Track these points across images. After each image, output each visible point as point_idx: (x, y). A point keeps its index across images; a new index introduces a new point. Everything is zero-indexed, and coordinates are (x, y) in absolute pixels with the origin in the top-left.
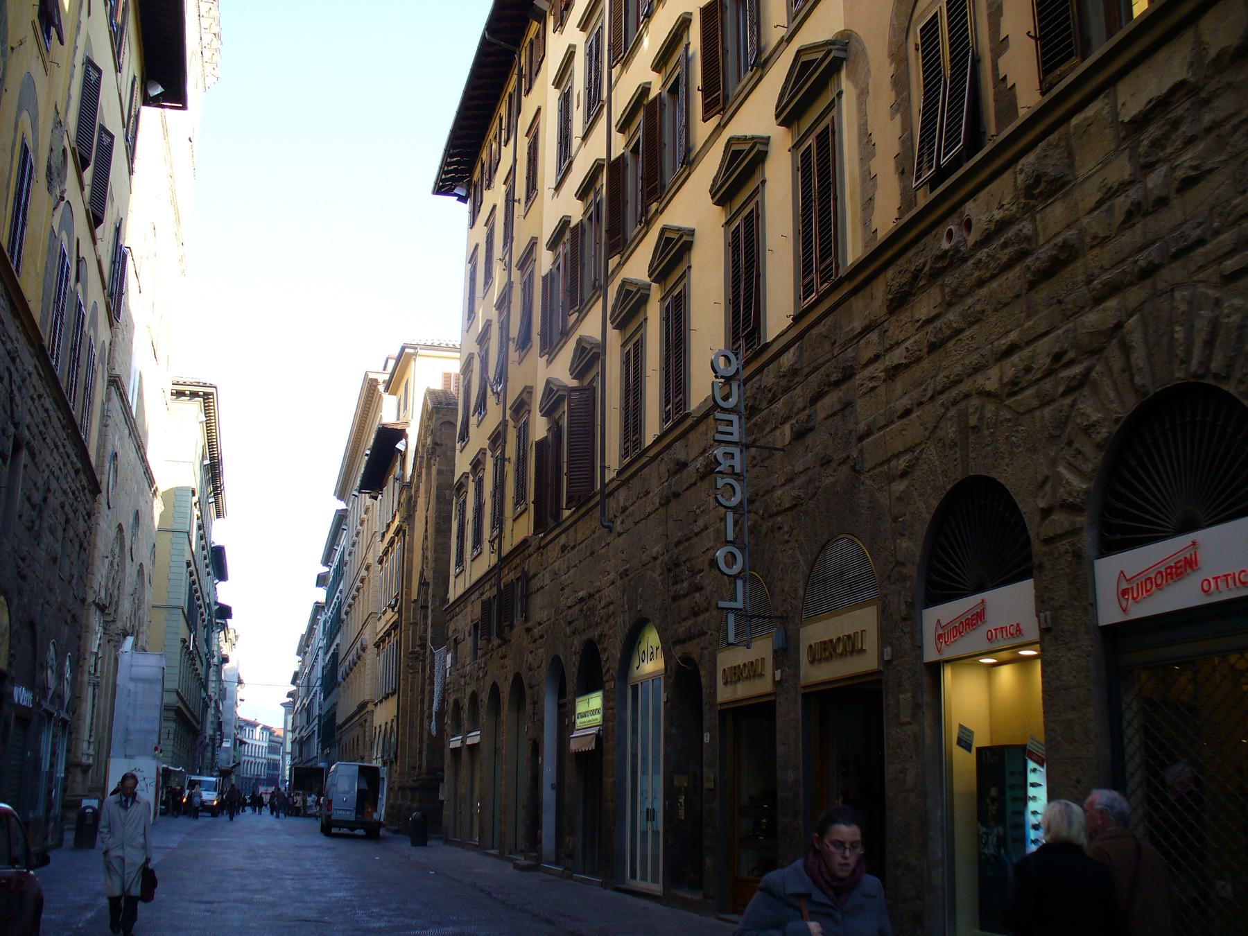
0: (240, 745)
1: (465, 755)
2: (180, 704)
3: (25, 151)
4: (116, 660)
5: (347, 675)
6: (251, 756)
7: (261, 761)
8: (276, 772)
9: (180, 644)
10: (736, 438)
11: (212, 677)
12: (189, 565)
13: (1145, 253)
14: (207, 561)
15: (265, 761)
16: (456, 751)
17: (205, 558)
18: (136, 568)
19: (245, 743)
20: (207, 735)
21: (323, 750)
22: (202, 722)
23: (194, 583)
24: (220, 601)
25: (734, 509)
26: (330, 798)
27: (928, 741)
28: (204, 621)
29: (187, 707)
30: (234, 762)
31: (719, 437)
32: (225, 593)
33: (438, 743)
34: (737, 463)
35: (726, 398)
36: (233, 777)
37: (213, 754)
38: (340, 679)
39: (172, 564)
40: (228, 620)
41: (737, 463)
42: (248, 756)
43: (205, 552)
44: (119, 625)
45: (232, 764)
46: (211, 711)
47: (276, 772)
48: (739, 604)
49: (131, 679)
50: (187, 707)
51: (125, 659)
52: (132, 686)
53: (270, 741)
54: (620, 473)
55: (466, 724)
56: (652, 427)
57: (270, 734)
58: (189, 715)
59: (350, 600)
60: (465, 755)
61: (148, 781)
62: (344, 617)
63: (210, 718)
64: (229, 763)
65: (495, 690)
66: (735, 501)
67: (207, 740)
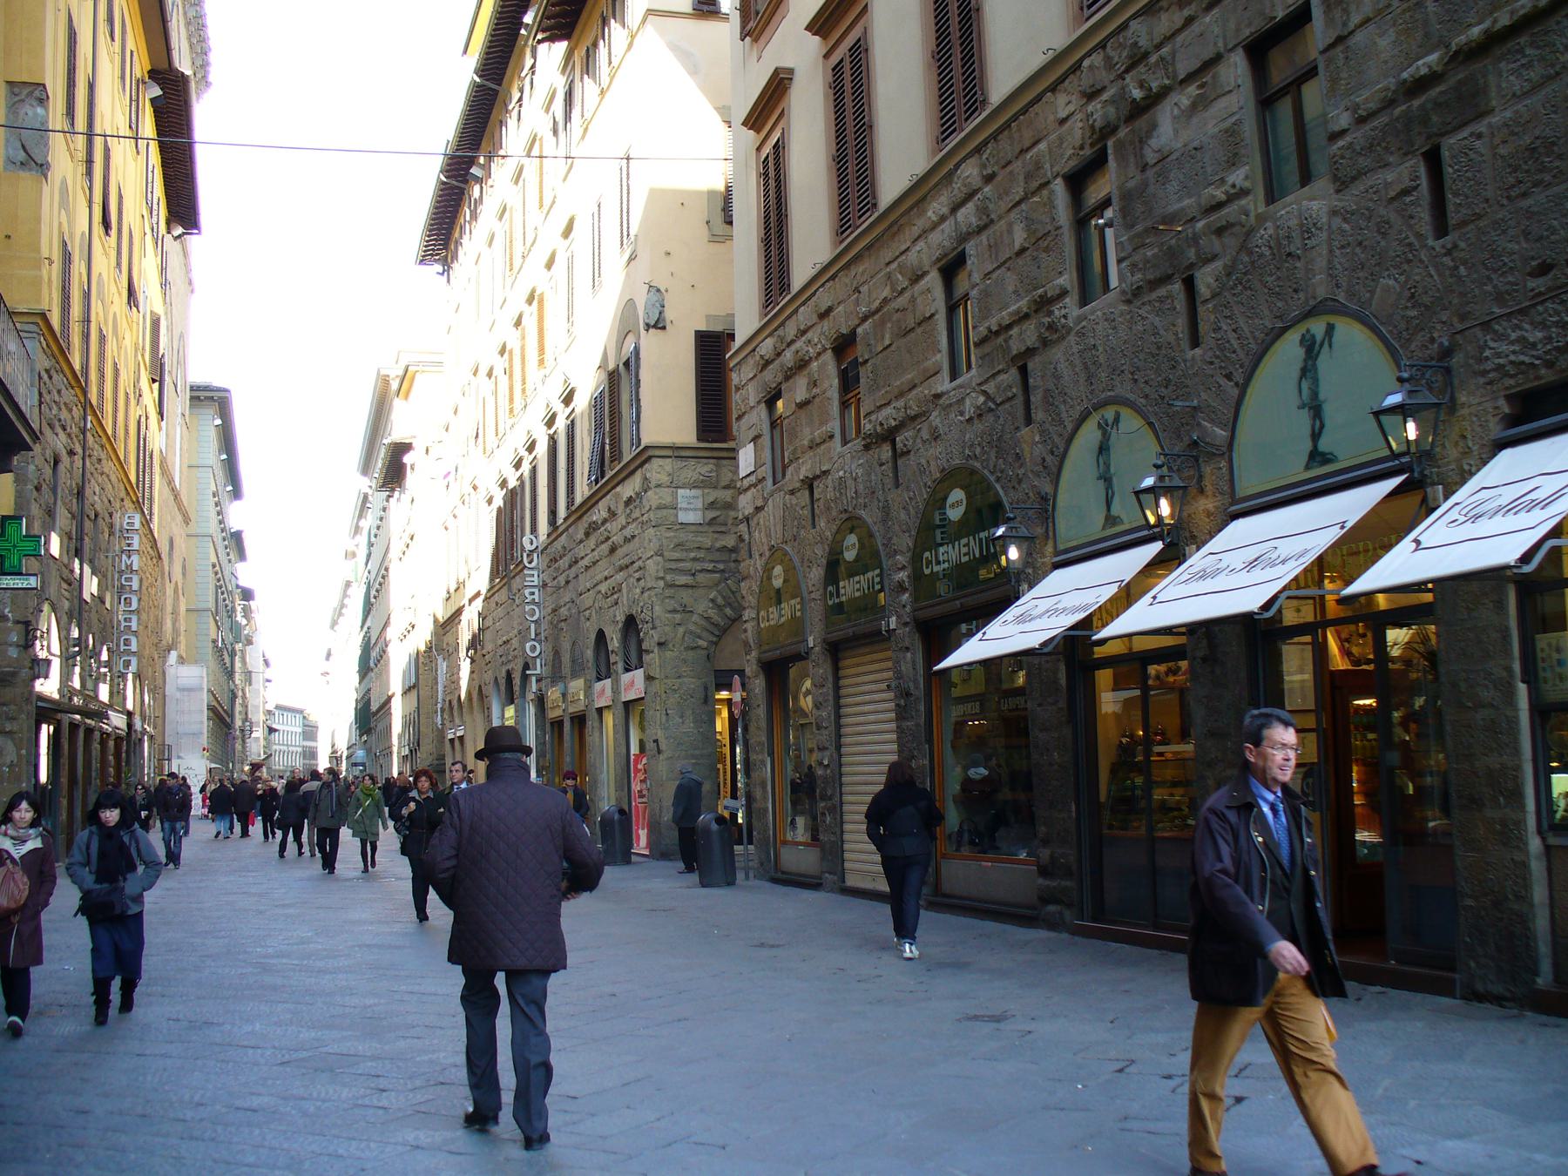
0: (270, 733)
1: (457, 743)
2: (215, 703)
3: (65, 244)
4: (164, 673)
5: (379, 661)
6: (283, 745)
7: (294, 749)
8: (314, 762)
9: (211, 645)
10: (536, 583)
11: (238, 665)
12: (214, 566)
13: (748, 479)
14: (226, 543)
15: (300, 750)
16: (452, 741)
17: (224, 540)
18: (173, 585)
19: (276, 730)
20: (237, 727)
21: (361, 736)
22: (232, 716)
23: (219, 580)
24: (241, 583)
25: (536, 622)
26: (1351, 986)
27: (597, 744)
28: (226, 606)
29: (220, 705)
30: (265, 753)
31: (526, 584)
32: (245, 574)
33: (441, 734)
34: (536, 597)
35: (530, 563)
36: (264, 769)
37: (244, 747)
38: (372, 665)
39: (198, 568)
40: (251, 602)
41: (536, 597)
42: (279, 744)
43: (224, 534)
44: (164, 642)
45: (263, 757)
46: (239, 701)
47: (314, 762)
48: (538, 671)
49: (179, 689)
50: (220, 705)
51: (170, 672)
52: (178, 695)
53: (305, 726)
54: (565, 519)
55: (457, 721)
56: (562, 512)
57: (304, 717)
58: (223, 713)
59: (380, 579)
60: (457, 743)
61: (199, 777)
62: (373, 600)
63: (238, 708)
64: (260, 756)
65: (509, 674)
66: (535, 618)
67: (238, 733)
